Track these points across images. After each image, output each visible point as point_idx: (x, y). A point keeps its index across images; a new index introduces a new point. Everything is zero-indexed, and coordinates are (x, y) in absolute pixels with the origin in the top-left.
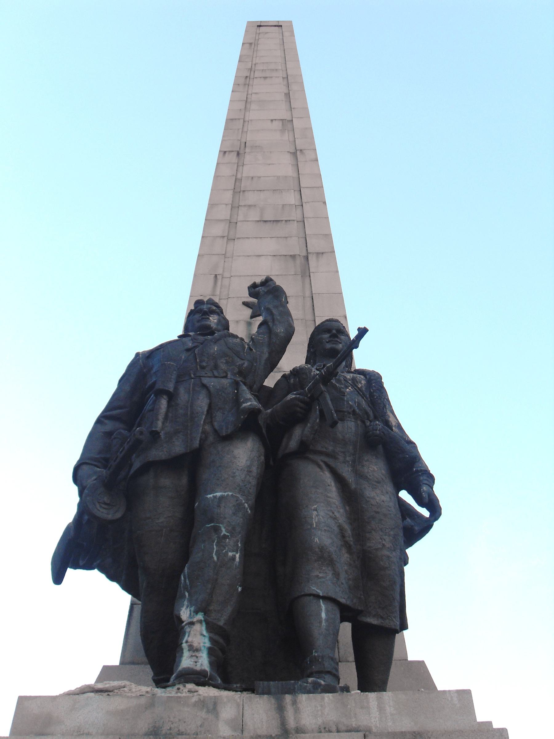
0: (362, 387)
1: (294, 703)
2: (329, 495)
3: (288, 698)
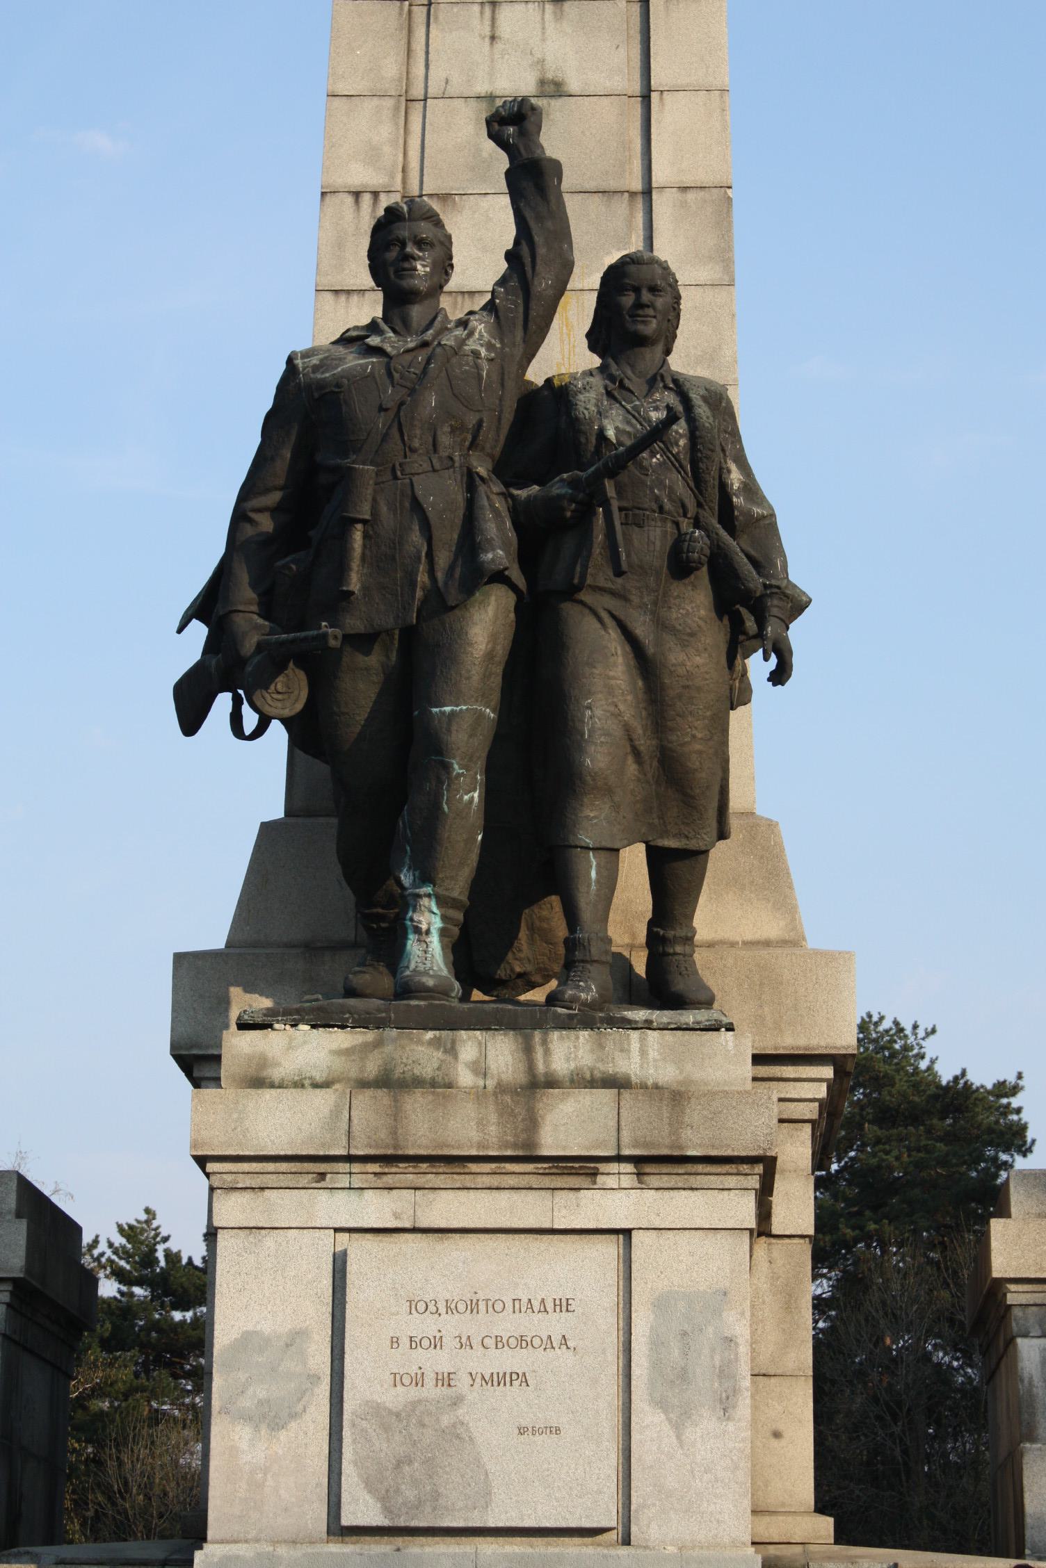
0: (678, 453)
1: (545, 1042)
2: (611, 673)
3: (537, 1035)
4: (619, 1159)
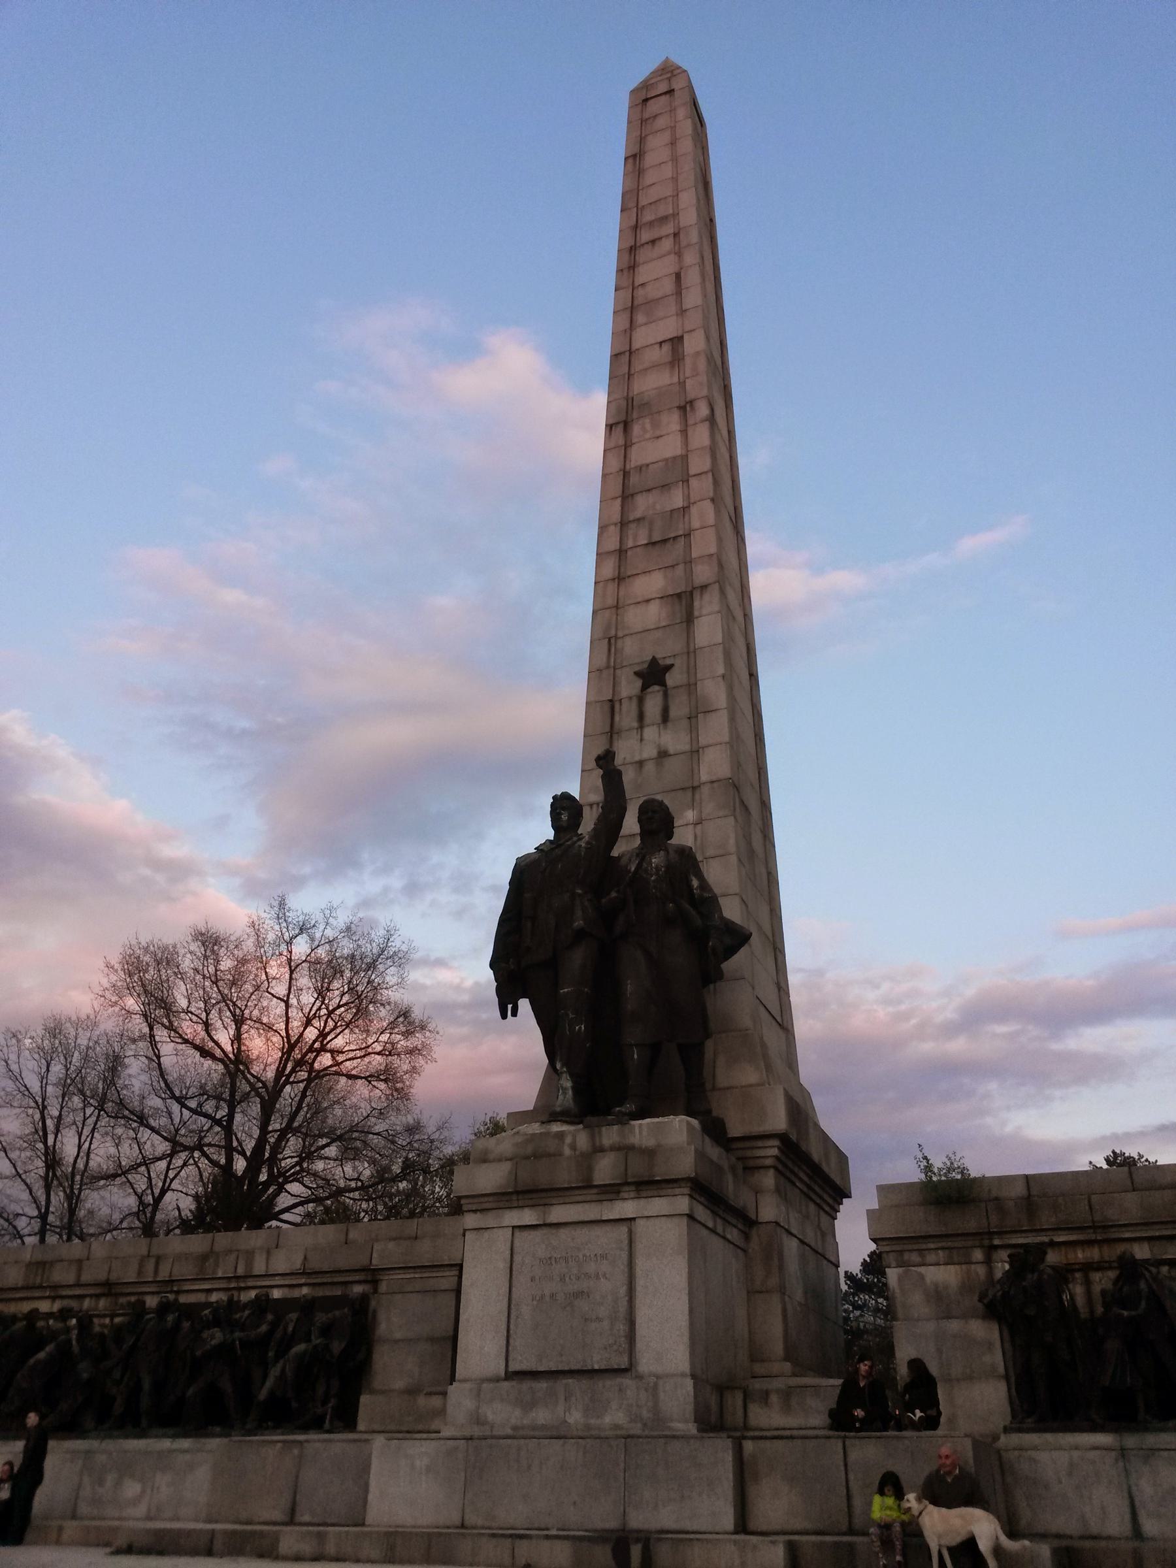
4: (627, 1184)
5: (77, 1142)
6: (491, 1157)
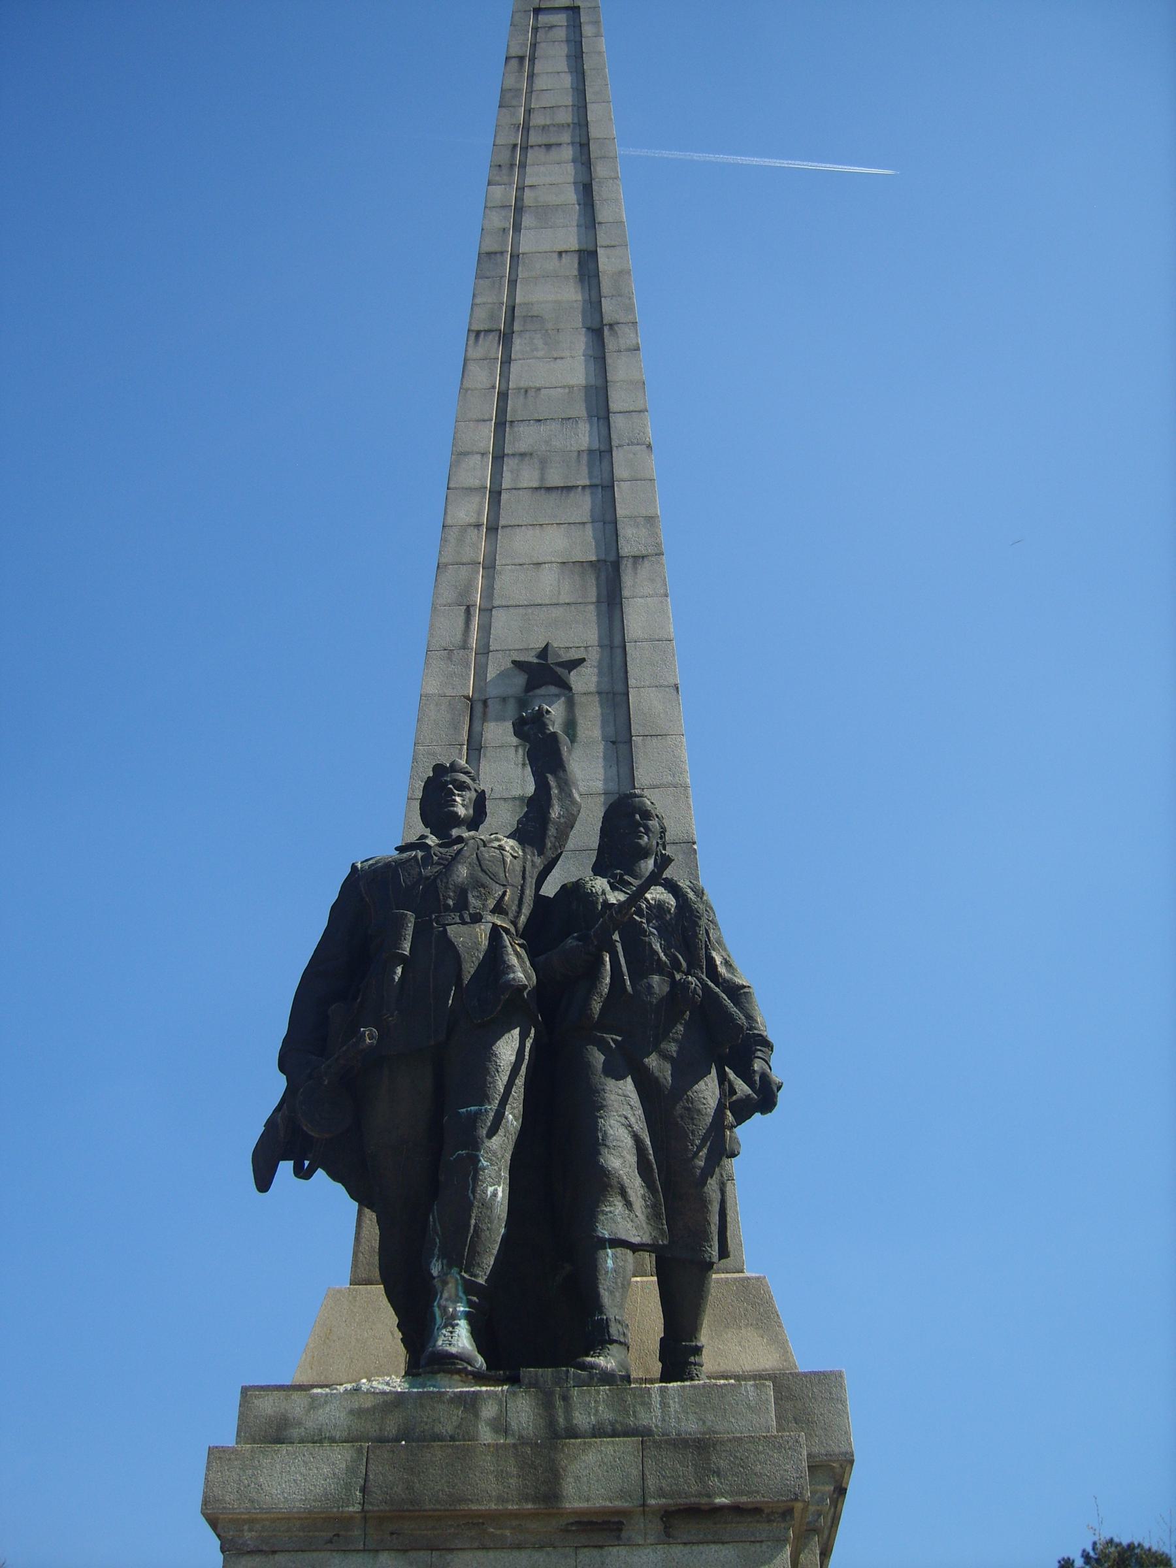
5: (530, 532)
6: (295, 1432)
